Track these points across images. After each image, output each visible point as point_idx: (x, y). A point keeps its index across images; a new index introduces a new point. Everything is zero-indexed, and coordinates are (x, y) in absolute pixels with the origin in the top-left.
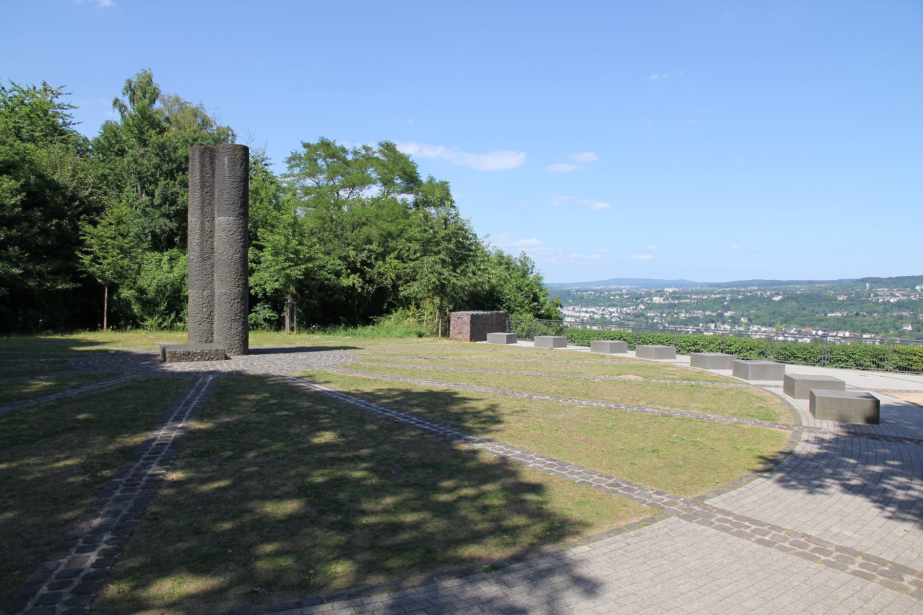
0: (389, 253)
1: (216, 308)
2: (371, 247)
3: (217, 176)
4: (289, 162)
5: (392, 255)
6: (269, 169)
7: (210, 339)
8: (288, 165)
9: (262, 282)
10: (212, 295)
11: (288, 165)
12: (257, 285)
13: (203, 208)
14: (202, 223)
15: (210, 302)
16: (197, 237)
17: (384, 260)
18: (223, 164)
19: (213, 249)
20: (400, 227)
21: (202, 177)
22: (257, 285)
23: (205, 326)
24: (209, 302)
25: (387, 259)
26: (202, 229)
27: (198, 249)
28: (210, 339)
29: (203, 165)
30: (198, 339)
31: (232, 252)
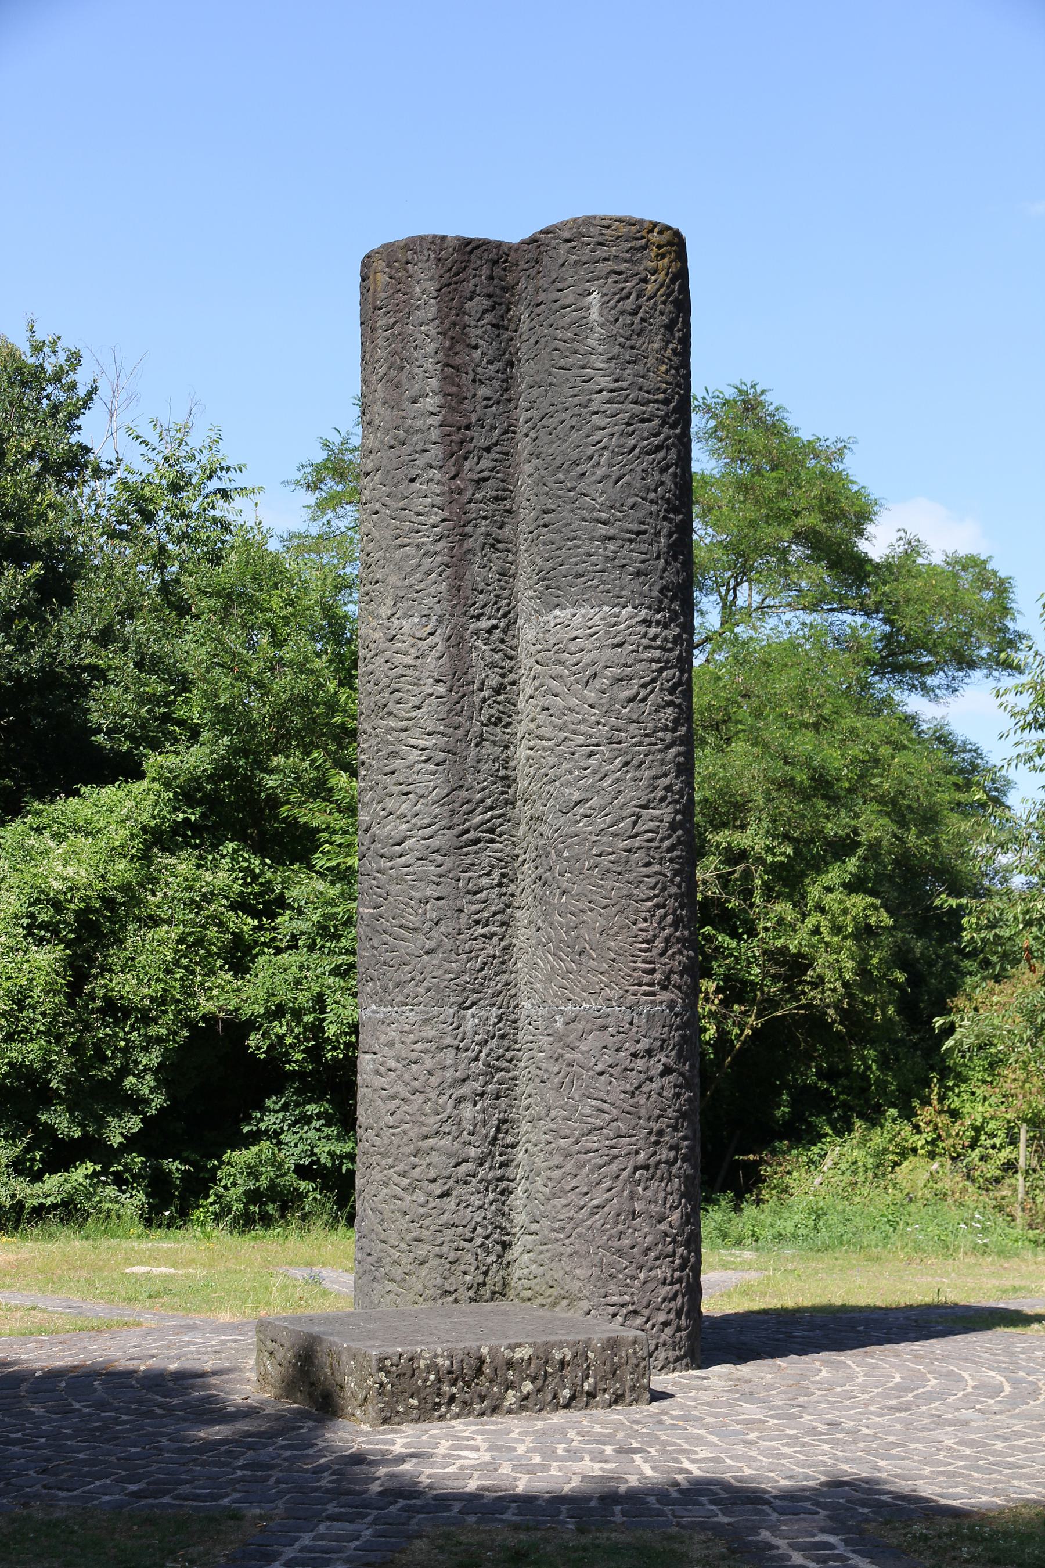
0: (818, 866)
1: (531, 1098)
2: (743, 840)
3: (524, 392)
4: (312, 487)
5: (834, 875)
6: (239, 512)
7: (494, 1279)
8: (311, 498)
9: (303, 999)
10: (506, 1031)
11: (311, 498)
12: (279, 1012)
13: (456, 565)
14: (457, 642)
15: (494, 1070)
16: (428, 717)
17: (798, 901)
18: (581, 325)
19: (507, 781)
20: (855, 750)
21: (454, 398)
22: (279, 1012)
23: (470, 1205)
24: (491, 1070)
25: (814, 892)
26: (458, 676)
27: (430, 782)
28: (494, 1279)
29: (454, 338)
30: (429, 1277)
31: (634, 795)
